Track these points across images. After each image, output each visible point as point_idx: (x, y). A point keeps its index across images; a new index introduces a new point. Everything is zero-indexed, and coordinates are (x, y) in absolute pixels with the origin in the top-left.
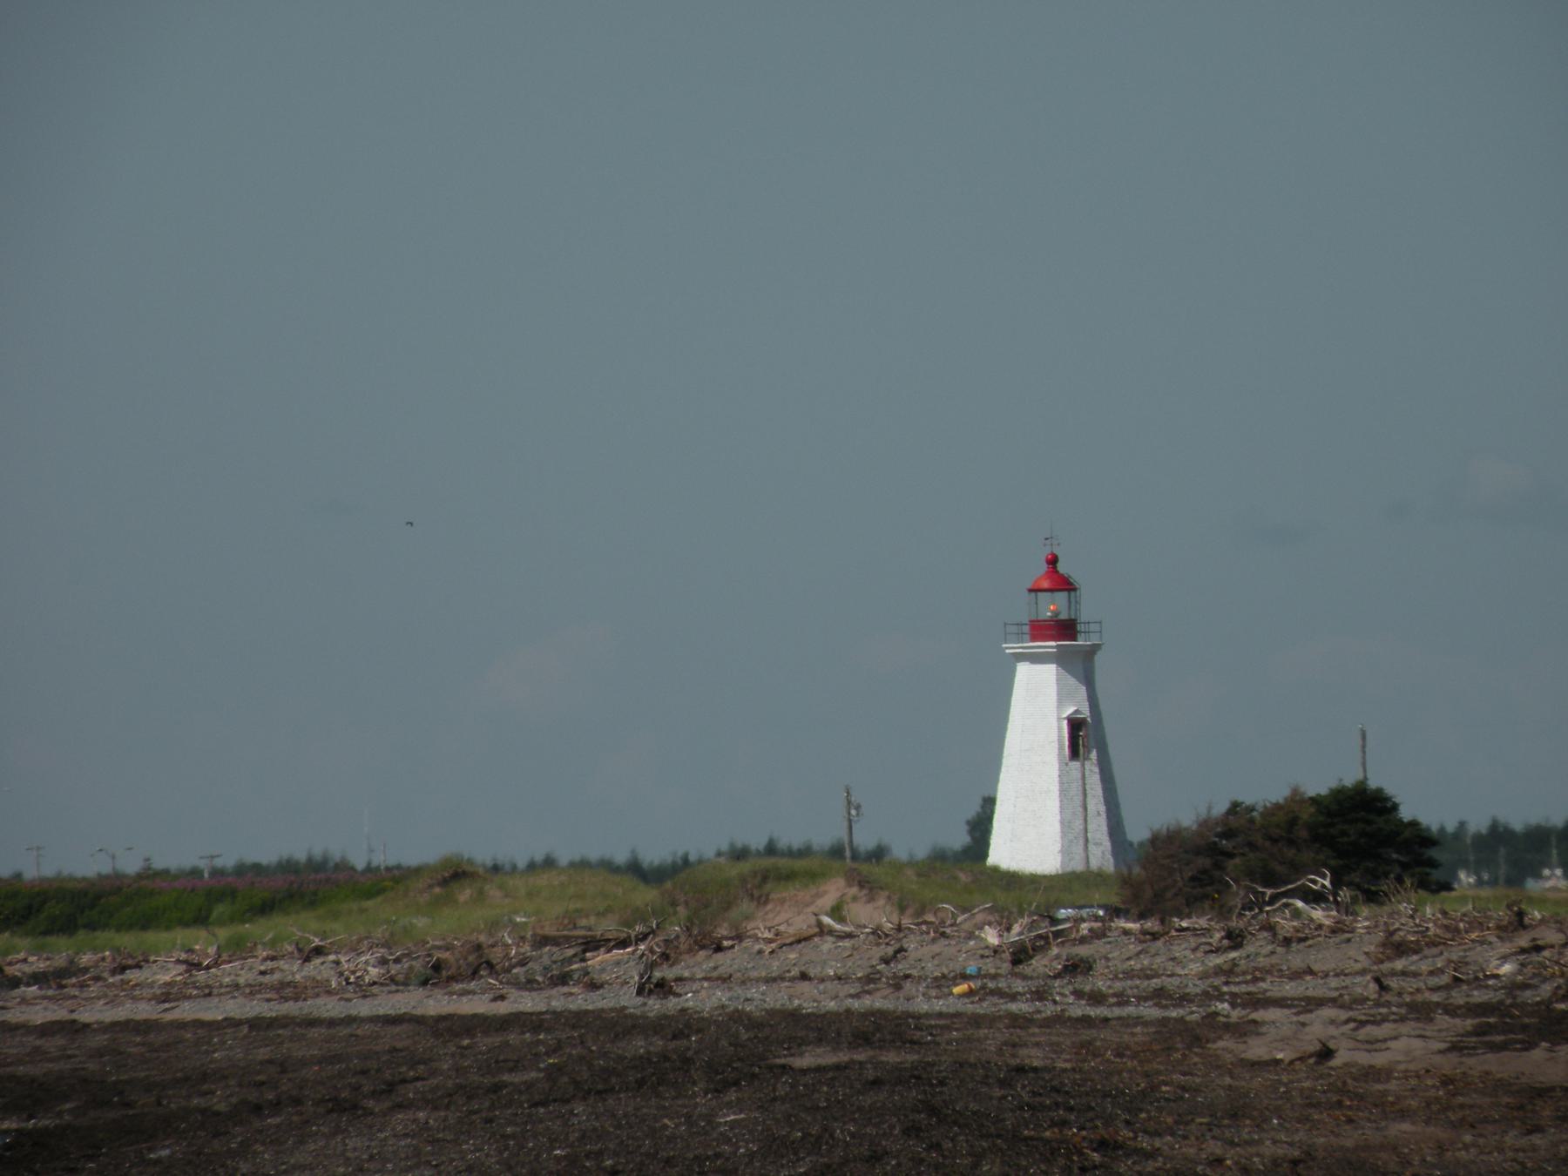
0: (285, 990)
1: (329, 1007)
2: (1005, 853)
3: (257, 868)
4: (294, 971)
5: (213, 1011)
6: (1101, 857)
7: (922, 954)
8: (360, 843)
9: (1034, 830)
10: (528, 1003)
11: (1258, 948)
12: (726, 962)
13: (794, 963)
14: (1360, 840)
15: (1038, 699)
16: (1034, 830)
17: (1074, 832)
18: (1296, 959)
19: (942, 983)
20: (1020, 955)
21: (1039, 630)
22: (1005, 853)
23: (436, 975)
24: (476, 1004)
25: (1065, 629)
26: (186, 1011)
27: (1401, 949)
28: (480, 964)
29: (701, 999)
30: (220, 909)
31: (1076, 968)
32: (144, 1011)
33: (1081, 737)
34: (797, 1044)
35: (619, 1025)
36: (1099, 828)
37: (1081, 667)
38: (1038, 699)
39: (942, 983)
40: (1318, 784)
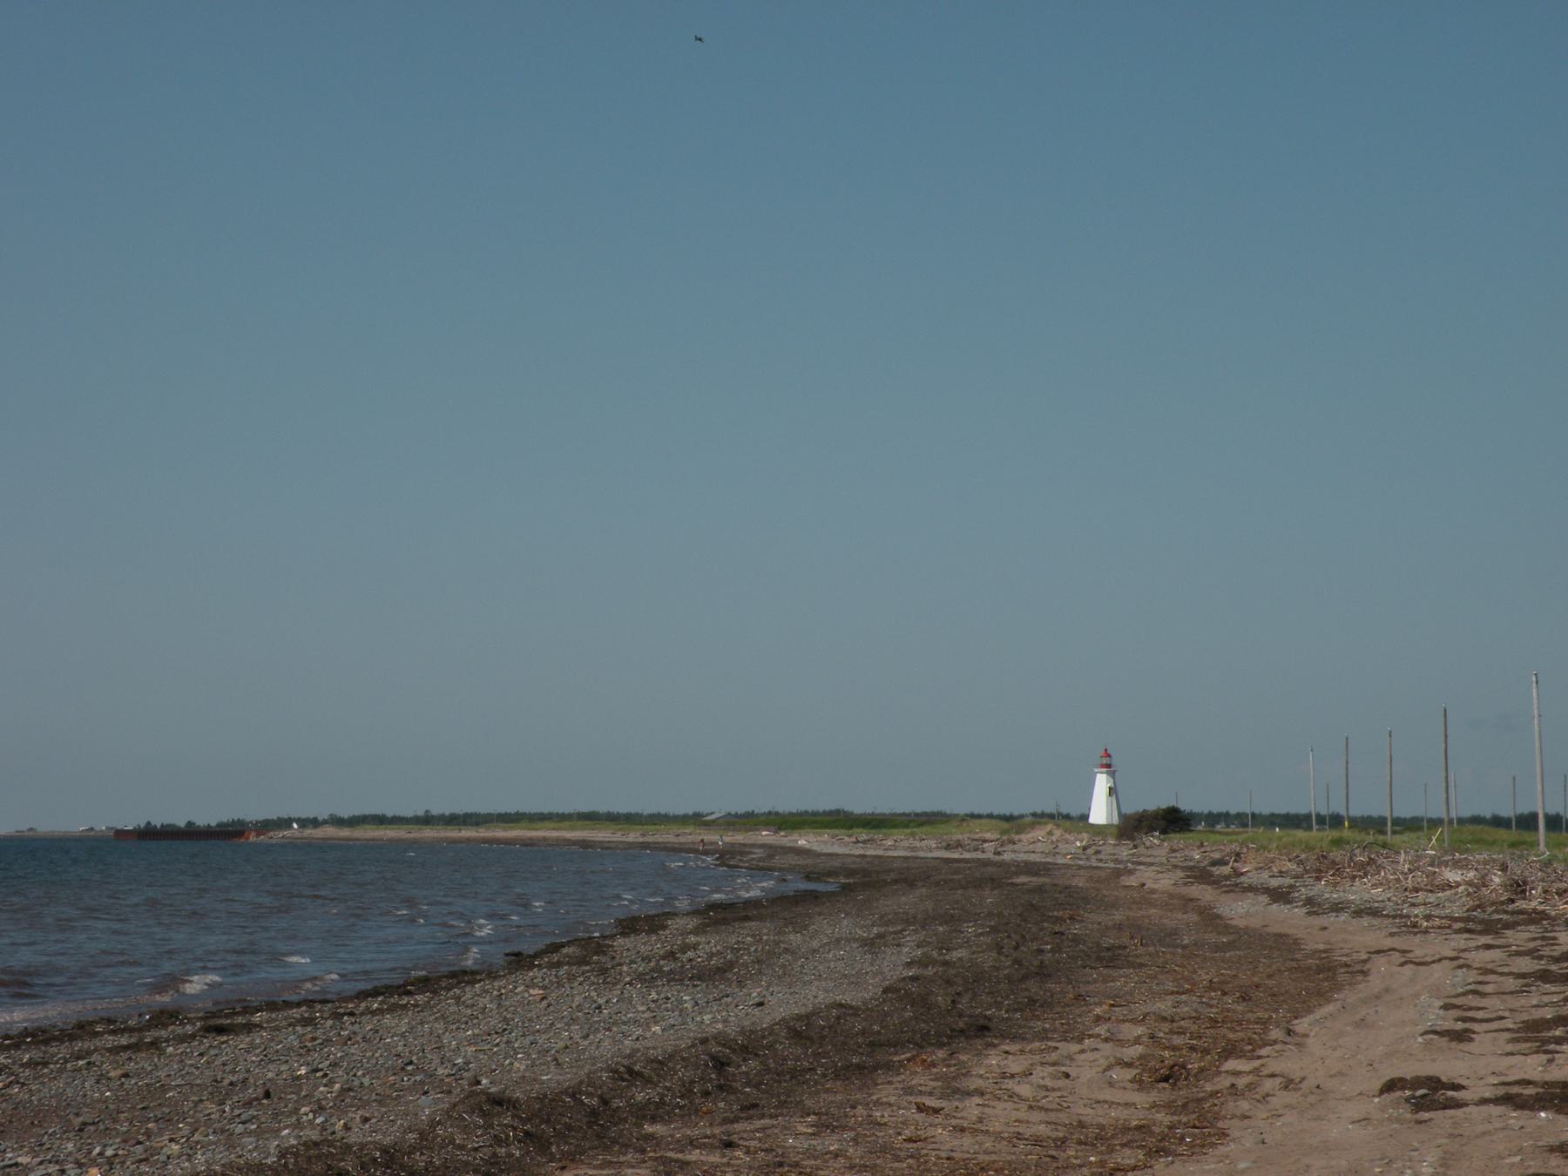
0: (913, 849)
1: (922, 854)
2: (1092, 820)
3: (777, 813)
4: (918, 844)
5: (895, 854)
6: (1116, 820)
7: (1062, 847)
8: (947, 809)
9: (1100, 812)
10: (967, 855)
11: (1141, 849)
12: (1016, 847)
13: (1034, 845)
14: (1173, 821)
15: (1102, 782)
16: (1100, 812)
17: (1110, 814)
18: (1150, 852)
19: (1065, 855)
20: (1085, 848)
21: (1103, 766)
22: (1092, 820)
23: (948, 847)
24: (956, 856)
25: (1109, 766)
26: (891, 853)
27: (1174, 851)
28: (959, 845)
29: (1007, 857)
30: (1029, 819)
31: (1098, 852)
32: (880, 852)
33: (1112, 791)
34: (1017, 874)
35: (986, 863)
36: (1116, 813)
37: (1112, 774)
38: (1102, 782)
39: (1065, 855)
40: (1164, 806)
